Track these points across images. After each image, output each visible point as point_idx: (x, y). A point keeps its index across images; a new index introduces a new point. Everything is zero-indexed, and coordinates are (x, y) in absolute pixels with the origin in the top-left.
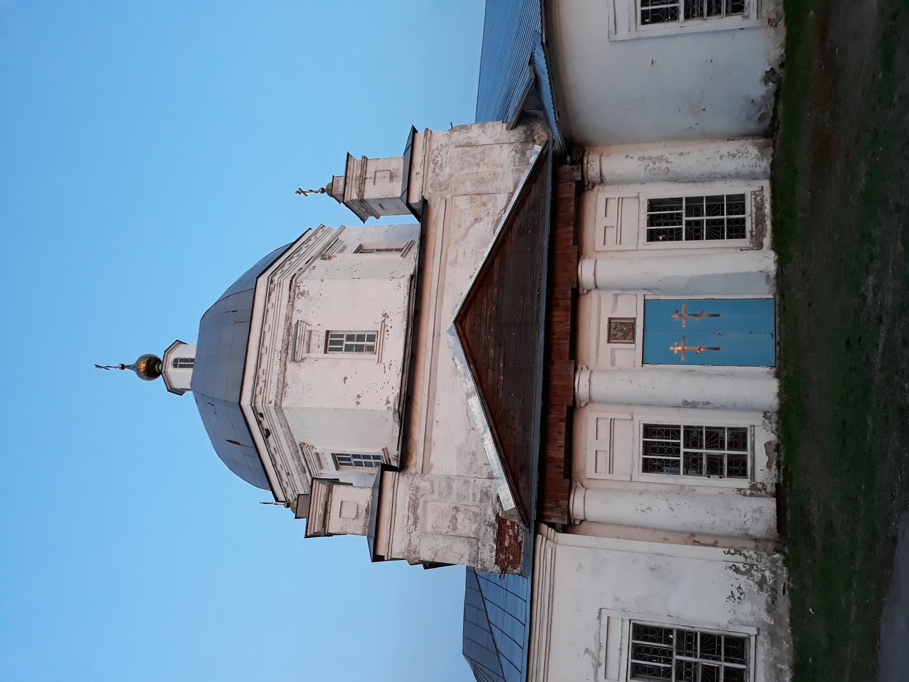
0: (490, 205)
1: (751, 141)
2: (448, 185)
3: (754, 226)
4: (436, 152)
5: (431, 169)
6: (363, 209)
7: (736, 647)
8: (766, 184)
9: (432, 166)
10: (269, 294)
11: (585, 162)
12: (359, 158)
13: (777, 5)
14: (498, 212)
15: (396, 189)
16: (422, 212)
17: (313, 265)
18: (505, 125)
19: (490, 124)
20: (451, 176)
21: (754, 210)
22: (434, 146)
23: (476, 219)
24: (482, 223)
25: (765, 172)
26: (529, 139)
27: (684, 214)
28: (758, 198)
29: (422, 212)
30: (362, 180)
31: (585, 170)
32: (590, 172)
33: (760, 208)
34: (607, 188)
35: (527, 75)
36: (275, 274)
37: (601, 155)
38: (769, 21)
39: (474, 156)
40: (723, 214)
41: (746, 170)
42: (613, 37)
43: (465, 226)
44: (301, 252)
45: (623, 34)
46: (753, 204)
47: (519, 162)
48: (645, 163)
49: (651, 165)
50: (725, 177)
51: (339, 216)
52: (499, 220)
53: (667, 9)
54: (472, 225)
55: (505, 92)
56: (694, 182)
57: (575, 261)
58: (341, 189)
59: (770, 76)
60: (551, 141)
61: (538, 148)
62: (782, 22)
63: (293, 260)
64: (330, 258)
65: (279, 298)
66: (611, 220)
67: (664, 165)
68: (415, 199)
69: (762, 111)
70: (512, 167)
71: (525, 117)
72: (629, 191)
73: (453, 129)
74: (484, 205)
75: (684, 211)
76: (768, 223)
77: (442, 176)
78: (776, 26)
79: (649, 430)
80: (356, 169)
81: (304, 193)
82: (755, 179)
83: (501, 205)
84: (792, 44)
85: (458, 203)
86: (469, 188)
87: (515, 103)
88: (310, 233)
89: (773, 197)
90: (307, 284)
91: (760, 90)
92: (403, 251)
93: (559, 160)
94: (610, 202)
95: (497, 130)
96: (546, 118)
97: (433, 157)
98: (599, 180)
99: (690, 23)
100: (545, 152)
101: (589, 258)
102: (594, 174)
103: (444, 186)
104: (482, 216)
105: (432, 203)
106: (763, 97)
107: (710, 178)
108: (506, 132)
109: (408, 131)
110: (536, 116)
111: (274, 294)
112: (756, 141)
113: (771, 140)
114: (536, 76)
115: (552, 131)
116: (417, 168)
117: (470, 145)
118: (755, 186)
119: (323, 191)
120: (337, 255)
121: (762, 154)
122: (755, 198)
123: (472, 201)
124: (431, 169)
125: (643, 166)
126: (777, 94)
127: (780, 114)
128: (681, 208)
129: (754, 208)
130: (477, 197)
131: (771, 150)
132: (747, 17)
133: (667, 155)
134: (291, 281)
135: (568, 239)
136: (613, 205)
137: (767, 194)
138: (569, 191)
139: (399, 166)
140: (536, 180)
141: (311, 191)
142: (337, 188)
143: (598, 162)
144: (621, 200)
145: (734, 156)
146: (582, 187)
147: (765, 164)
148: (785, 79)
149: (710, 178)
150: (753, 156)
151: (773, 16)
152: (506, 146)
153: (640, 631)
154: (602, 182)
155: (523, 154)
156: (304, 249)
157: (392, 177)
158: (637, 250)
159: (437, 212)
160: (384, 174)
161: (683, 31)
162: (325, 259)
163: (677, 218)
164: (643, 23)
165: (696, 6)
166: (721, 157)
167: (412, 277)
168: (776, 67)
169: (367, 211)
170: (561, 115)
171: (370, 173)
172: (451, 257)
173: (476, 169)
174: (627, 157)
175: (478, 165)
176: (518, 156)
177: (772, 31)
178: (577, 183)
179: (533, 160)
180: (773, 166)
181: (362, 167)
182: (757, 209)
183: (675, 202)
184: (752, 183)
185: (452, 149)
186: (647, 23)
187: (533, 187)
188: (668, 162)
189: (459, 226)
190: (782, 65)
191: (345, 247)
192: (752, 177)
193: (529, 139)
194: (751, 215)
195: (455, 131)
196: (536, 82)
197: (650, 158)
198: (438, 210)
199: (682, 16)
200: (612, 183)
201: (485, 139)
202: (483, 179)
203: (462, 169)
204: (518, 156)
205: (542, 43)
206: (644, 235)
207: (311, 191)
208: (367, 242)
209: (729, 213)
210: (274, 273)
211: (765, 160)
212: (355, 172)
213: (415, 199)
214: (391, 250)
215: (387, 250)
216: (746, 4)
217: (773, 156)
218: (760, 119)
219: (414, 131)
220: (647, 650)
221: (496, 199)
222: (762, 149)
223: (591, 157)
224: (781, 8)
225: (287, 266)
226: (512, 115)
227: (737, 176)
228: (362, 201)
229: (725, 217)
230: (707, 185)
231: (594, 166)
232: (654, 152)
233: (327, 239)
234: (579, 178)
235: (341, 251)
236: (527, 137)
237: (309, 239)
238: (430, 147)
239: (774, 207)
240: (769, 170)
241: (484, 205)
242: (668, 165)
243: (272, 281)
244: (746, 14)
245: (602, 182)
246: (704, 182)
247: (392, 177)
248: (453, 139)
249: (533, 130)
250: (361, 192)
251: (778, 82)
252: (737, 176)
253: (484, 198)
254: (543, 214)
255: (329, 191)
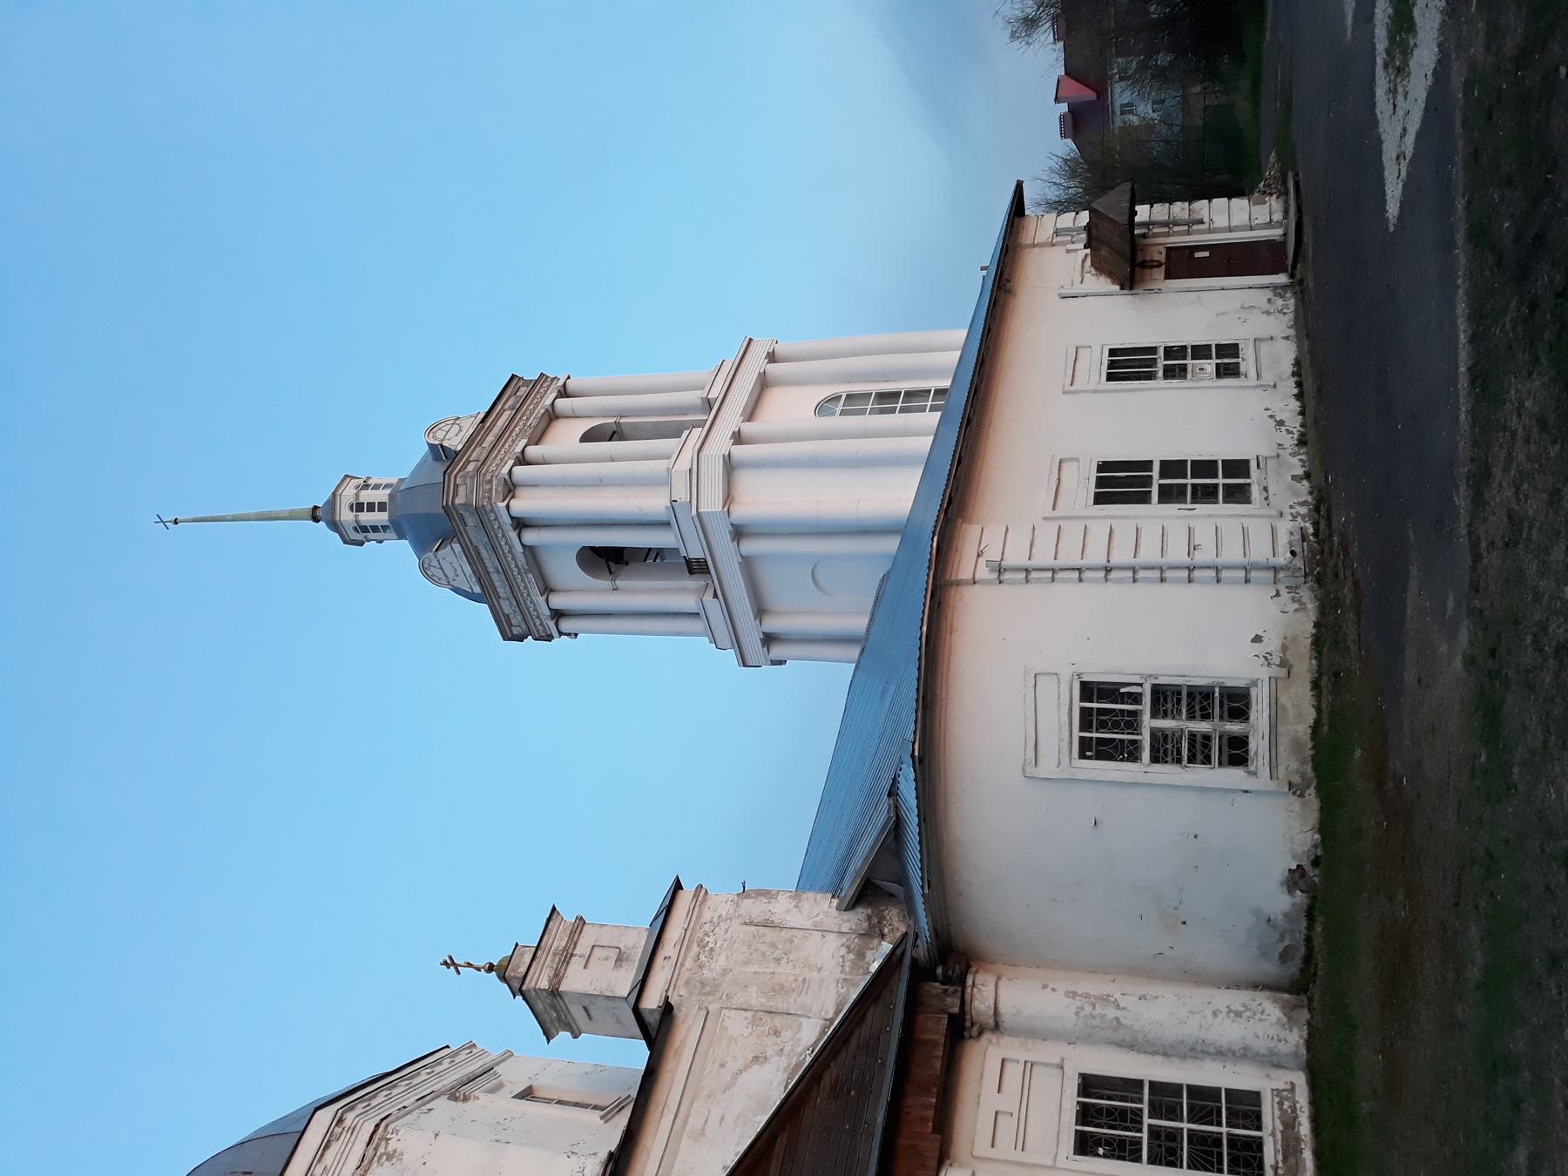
0: (787, 1035)
1: (1268, 993)
2: (718, 986)
3: (1280, 1157)
4: (707, 927)
5: (692, 954)
6: (554, 1013)
7: (1246, 1107)
8: (1300, 1079)
9: (695, 949)
10: (326, 1146)
11: (969, 982)
12: (570, 918)
13: (1303, 763)
14: (799, 1050)
15: (623, 983)
16: (656, 1030)
17: (428, 1106)
18: (835, 901)
19: (810, 895)
20: (725, 971)
21: (1280, 1127)
22: (707, 916)
23: (756, 1058)
24: (766, 1067)
25: (1296, 1054)
26: (874, 931)
27: (1146, 1111)
28: (1286, 1105)
29: (656, 1030)
30: (567, 956)
31: (967, 997)
32: (976, 1003)
33: (1290, 1124)
34: (1005, 1040)
35: (882, 815)
36: (352, 1108)
37: (999, 978)
38: (1290, 785)
39: (773, 945)
40: (1219, 1124)
41: (1261, 1045)
42: (1030, 770)
43: (733, 1066)
44: (415, 1081)
45: (1048, 767)
46: (1277, 1113)
47: (852, 969)
48: (1077, 1003)
49: (1088, 1009)
50: (1222, 1054)
51: (507, 1023)
52: (797, 1066)
53: (1122, 741)
54: (747, 1067)
55: (843, 848)
56: (1165, 1055)
57: (934, 1164)
58: (523, 969)
59: (1295, 879)
60: (911, 933)
61: (887, 947)
62: (1312, 791)
63: (395, 1091)
64: (466, 1099)
65: (342, 1157)
66: (1009, 1101)
67: (1111, 1013)
68: (652, 1001)
69: (1287, 943)
70: (837, 974)
71: (870, 892)
72: (1048, 1052)
73: (744, 894)
74: (777, 1033)
75: (1145, 1107)
76: (1308, 1155)
77: (711, 970)
78: (1302, 795)
79: (1089, 1084)
80: (562, 935)
81: (456, 966)
82: (1278, 1066)
83: (805, 1037)
84: (1326, 827)
85: (727, 1022)
86: (755, 998)
87: (858, 863)
88: (446, 1051)
89: (1314, 1102)
90: (407, 1139)
91: (1281, 903)
92: (607, 1112)
93: (921, 974)
94: (1009, 1067)
95: (823, 908)
96: (909, 898)
97: (700, 935)
98: (991, 1021)
99: (1158, 767)
100: (898, 952)
101: (961, 1166)
102: (982, 1007)
103: (709, 988)
104: (769, 1052)
105: (680, 1014)
106: (1286, 915)
107: (1195, 1051)
108: (836, 913)
109: (668, 884)
110: (891, 895)
111: (334, 1148)
112: (1278, 995)
113: (1304, 997)
114: (898, 817)
115: (916, 922)
116: (669, 948)
117: (768, 924)
118: (1281, 1080)
119: (491, 968)
120: (482, 1096)
121: (1290, 1019)
122: (1281, 1104)
123: (755, 1022)
124: (692, 954)
125: (1074, 1009)
126: (1310, 914)
127: (1317, 942)
128: (1141, 1101)
129: (1278, 1122)
130: (767, 1017)
131: (1305, 1015)
132: (1254, 774)
133: (1117, 995)
134: (377, 1126)
135: (924, 1120)
136: (1014, 1073)
137: (1302, 1098)
138: (935, 1029)
139: (638, 944)
140: (876, 999)
141: (469, 965)
142: (518, 966)
143: (992, 988)
144: (1029, 1066)
145: (1238, 1014)
146: (960, 1030)
147: (1294, 1040)
148: (1324, 883)
149: (1195, 1051)
150: (1273, 1019)
151: (1296, 779)
152: (831, 936)
153: (1089, 690)
154: (997, 1027)
155: (861, 955)
156: (423, 1076)
157: (621, 959)
158: (1053, 1167)
159: (686, 1033)
160: (605, 952)
161: (1148, 779)
162: (456, 1099)
163: (1133, 1121)
164: (1082, 756)
165: (1169, 706)
166: (1215, 1014)
167: (611, 1154)
168: (1306, 863)
169: (559, 1019)
170: (933, 884)
171: (583, 947)
172: (694, 1123)
173: (772, 966)
174: (1045, 987)
175: (778, 961)
176: (852, 956)
177: (1296, 803)
178: (951, 1016)
179: (875, 967)
180: (1310, 1043)
181: (572, 933)
182: (1284, 1124)
183: (1132, 1087)
184: (1274, 1073)
185: (736, 926)
186: (1089, 758)
187: (871, 1011)
188: (1118, 1007)
189: (722, 1066)
190: (1316, 862)
191: (500, 1086)
192: (1272, 1061)
193: (874, 931)
194: (1273, 1134)
195: (749, 897)
196: (896, 827)
197: (1087, 996)
198: (689, 1028)
199: (1146, 755)
200: (1016, 1032)
201: (795, 919)
202: (782, 986)
203: (746, 963)
204: (852, 956)
205: (913, 756)
206: (1069, 1142)
207: (469, 965)
208: (543, 1084)
209: (1229, 1125)
210: (350, 1107)
211: (1295, 1030)
212: (558, 940)
213: (652, 1001)
214: (585, 1106)
215: (576, 1105)
216: (1251, 754)
217: (1309, 1024)
218: (1284, 956)
219: (678, 886)
220: (1116, 726)
221: (801, 1025)
222: (1289, 1010)
223: (980, 978)
224: (1309, 768)
225: (381, 1098)
226: (849, 888)
227: (1243, 1055)
228: (554, 993)
229: (1224, 1129)
230: (1190, 1064)
231: (984, 993)
232: (1095, 986)
233: (475, 1066)
234: (956, 1010)
235: (493, 1091)
236: (871, 927)
237: (439, 1062)
238: (699, 917)
239: (1315, 1120)
240: (1304, 1051)
241: (777, 1033)
242: (1119, 1013)
243: (341, 1121)
244: (1252, 768)
245: (997, 1027)
246: (1184, 1057)
247: (621, 959)
248: (742, 911)
249: (883, 918)
250: (558, 976)
251: (1312, 892)
252: (1243, 1055)
253: (778, 1021)
254: (883, 1065)
255: (501, 970)
